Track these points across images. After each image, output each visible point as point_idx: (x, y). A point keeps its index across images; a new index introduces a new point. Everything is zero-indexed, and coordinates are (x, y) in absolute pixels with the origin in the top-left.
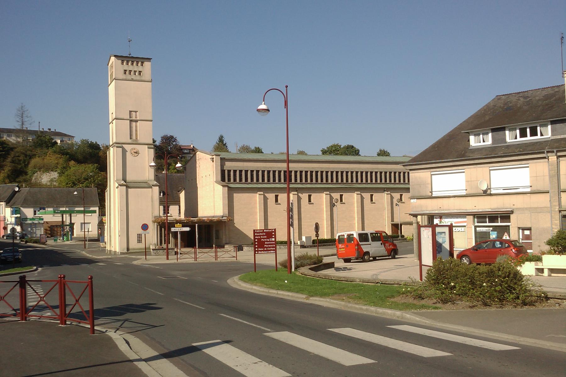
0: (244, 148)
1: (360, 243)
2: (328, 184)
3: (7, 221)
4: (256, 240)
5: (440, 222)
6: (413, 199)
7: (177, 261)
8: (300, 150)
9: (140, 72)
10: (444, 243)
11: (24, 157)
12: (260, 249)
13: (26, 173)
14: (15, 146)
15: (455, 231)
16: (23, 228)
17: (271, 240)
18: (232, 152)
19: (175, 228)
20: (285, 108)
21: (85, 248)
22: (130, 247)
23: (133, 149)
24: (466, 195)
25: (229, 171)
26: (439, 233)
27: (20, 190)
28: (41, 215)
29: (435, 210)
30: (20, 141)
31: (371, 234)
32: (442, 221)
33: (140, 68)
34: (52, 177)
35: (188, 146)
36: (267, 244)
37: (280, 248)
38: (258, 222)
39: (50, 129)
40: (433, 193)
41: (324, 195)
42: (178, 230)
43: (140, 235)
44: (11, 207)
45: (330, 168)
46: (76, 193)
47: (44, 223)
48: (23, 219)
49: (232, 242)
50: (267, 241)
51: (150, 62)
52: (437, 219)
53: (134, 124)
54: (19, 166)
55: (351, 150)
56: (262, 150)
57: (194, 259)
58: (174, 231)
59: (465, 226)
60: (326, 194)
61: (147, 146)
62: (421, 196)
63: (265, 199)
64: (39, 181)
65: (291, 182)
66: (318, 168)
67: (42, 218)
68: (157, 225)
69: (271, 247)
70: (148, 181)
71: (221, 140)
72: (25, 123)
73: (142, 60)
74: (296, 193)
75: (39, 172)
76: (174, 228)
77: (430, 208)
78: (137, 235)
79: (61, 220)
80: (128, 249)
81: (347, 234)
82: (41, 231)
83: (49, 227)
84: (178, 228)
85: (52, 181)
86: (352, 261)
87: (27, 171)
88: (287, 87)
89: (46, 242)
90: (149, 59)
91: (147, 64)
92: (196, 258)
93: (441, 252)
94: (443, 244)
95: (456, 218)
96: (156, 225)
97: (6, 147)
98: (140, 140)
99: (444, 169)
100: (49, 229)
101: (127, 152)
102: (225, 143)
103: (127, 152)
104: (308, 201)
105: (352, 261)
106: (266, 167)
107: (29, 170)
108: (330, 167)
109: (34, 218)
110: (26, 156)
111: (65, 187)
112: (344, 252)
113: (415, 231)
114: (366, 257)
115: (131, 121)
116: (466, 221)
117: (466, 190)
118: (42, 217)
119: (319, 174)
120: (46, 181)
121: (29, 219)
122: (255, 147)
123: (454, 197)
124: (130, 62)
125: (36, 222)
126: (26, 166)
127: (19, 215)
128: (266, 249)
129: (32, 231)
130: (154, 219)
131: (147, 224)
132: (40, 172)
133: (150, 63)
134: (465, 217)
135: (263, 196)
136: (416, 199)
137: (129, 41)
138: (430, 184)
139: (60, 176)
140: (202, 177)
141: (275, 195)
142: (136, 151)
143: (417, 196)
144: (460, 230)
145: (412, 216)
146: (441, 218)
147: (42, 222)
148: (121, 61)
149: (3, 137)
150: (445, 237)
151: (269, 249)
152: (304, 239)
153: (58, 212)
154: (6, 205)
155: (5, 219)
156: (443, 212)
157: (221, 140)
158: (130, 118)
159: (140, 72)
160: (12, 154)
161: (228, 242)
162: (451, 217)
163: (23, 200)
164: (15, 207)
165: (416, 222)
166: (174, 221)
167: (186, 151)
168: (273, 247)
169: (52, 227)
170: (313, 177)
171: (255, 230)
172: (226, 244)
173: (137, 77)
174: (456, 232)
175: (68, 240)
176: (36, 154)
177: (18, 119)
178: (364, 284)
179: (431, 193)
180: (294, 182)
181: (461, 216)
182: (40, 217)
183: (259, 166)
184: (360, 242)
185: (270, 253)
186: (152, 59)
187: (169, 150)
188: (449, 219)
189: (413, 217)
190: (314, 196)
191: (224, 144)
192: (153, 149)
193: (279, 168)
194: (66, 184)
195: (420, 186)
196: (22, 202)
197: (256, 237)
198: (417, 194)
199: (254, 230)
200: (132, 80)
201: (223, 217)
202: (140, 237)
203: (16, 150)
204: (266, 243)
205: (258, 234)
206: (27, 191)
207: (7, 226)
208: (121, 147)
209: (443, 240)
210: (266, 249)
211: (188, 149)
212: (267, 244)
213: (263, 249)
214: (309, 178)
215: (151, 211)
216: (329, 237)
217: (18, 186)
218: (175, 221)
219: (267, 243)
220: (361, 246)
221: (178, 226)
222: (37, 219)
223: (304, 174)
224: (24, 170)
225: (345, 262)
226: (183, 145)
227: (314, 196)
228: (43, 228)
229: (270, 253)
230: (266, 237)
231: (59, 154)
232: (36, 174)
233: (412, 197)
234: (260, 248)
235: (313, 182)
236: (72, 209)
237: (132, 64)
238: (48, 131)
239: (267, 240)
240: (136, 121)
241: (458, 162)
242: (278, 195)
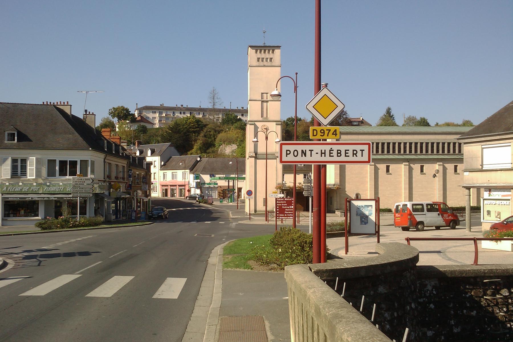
0: (411, 118)
1: (413, 213)
2: (445, 154)
3: (190, 185)
4: (278, 207)
5: (490, 195)
6: (465, 172)
7: (268, 223)
8: (466, 120)
9: (271, 59)
10: (371, 215)
11: (214, 133)
12: (281, 215)
13: (214, 145)
14: (208, 123)
15: (502, 204)
16: (202, 191)
17: (290, 207)
18: (432, 123)
20: (295, 92)
21: (238, 209)
22: (258, 209)
23: (264, 126)
24: (511, 169)
26: (366, 206)
27: (201, 160)
28: (215, 181)
29: (485, 183)
30: (212, 118)
31: (427, 205)
32: (491, 194)
33: (271, 55)
34: (233, 149)
35: (358, 119)
36: (287, 211)
37: (382, 215)
38: (368, 191)
39: (243, 108)
40: (484, 166)
41: (437, 165)
44: (193, 174)
45: (447, 139)
46: (231, 163)
47: (218, 187)
48: (203, 183)
50: (287, 209)
51: (280, 49)
52: (486, 191)
53: (265, 104)
54: (210, 140)
55: (424, 123)
56: (427, 121)
57: (281, 222)
59: (509, 200)
60: (404, 165)
61: (275, 123)
62: (473, 169)
63: (411, 170)
64: (223, 152)
65: (406, 153)
66: (434, 139)
67: (217, 183)
68: (280, 191)
69: (290, 214)
70: (275, 153)
71: (389, 111)
72: (216, 104)
73: (273, 48)
74: (407, 163)
75: (223, 145)
77: (480, 182)
78: (263, 199)
79: (232, 185)
80: (255, 211)
81: (402, 204)
82: (216, 194)
83: (222, 191)
85: (233, 152)
86: (410, 230)
87: (215, 144)
88: (297, 74)
89: (213, 203)
90: (278, 47)
91: (277, 52)
93: (368, 223)
94: (370, 217)
95: (503, 191)
96: (279, 191)
97: (201, 124)
98: (270, 118)
99: (489, 143)
100: (222, 192)
101: (258, 129)
102: (392, 115)
103: (259, 128)
104: (420, 172)
105: (410, 230)
106: (380, 140)
107: (217, 144)
108: (447, 138)
109: (210, 183)
110: (215, 131)
111: (240, 157)
112: (400, 221)
113: (467, 203)
114: (419, 226)
115: (263, 102)
116: (511, 195)
117: (512, 163)
118: (216, 182)
119: (435, 145)
120: (228, 152)
121: (206, 183)
122: (421, 118)
123: (501, 170)
124: (263, 51)
125: (212, 186)
126: (215, 139)
127: (199, 181)
128: (286, 215)
129: (208, 194)
130: (277, 186)
131: (251, 190)
132: (224, 144)
133: (280, 50)
134: (509, 191)
135: (408, 166)
136: (468, 172)
137: (264, 33)
138: (481, 158)
139: (238, 148)
141: (387, 166)
142: (266, 128)
143: (470, 169)
144: (506, 204)
145: (465, 189)
146: (490, 191)
147: (216, 186)
148: (255, 50)
149: (206, 116)
150: (372, 210)
151: (289, 215)
153: (223, 178)
154: (190, 171)
155: (189, 183)
156: (491, 185)
157: (389, 111)
158: (262, 99)
159: (271, 59)
160: (205, 130)
161: (339, 208)
162: (499, 191)
163: (203, 168)
164: (196, 174)
165: (469, 195)
166: (334, 188)
167: (355, 124)
168: (292, 214)
169: (224, 190)
170: (428, 148)
171: (277, 199)
172: (337, 210)
173: (269, 63)
174: (502, 205)
175: (231, 202)
176: (223, 129)
177: (210, 101)
179: (481, 166)
180: (408, 153)
181: (508, 190)
182: (215, 182)
183: (374, 138)
184: (413, 212)
185: (290, 218)
187: (340, 122)
188: (500, 192)
189: (466, 189)
190: (392, 167)
191: (391, 116)
192: (280, 125)
193: (394, 140)
194: (241, 155)
195: (472, 159)
196: (202, 169)
197: (278, 205)
198: (469, 167)
199: (276, 199)
200: (264, 66)
201: (334, 185)
203: (208, 127)
204: (286, 210)
205: (280, 202)
206: (206, 161)
207: (191, 189)
208: (253, 125)
209: (369, 213)
210: (286, 215)
211: (357, 121)
212: (287, 211)
213: (283, 215)
214: (435, 150)
216: (476, 205)
217: (200, 157)
218: (288, 188)
219: (287, 210)
220: (414, 216)
222: (213, 183)
223: (435, 145)
224: (214, 143)
225: (403, 231)
226: (352, 118)
227: (392, 167)
228: (217, 191)
229: (290, 218)
230: (286, 205)
231: (240, 129)
232: (221, 146)
233: (465, 170)
234: (281, 214)
235: (412, 153)
236: (228, 176)
237: (265, 52)
238: (241, 109)
239: (287, 207)
240: (267, 102)
241: (494, 137)
242: (389, 165)
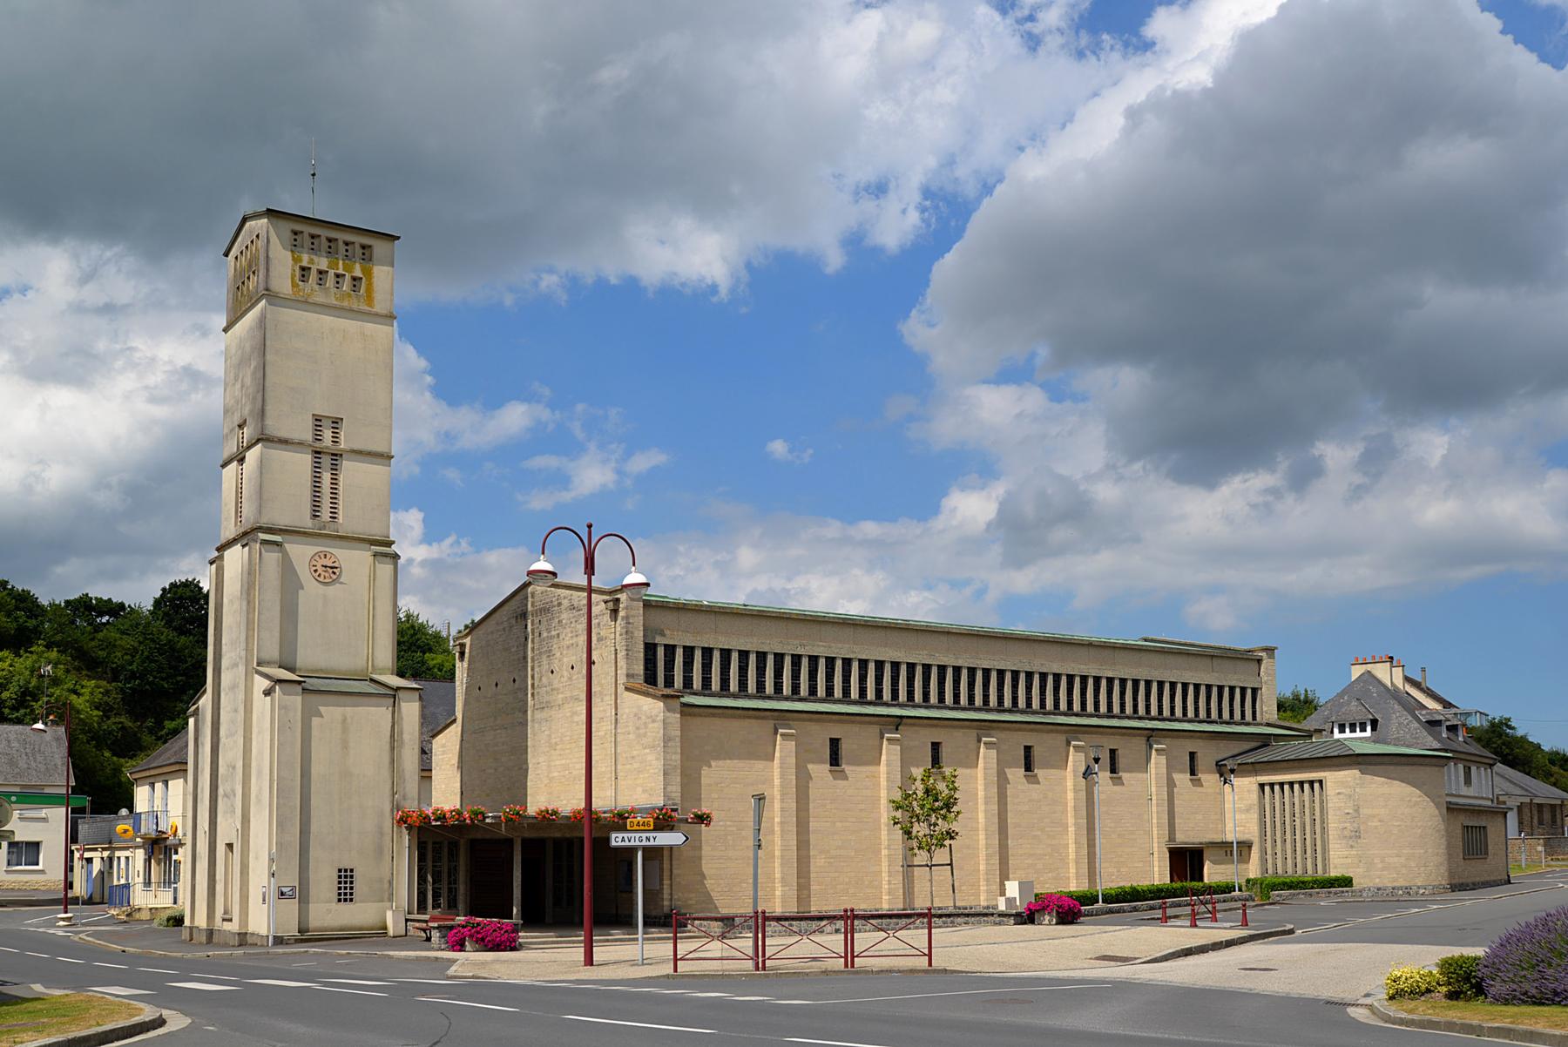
19: (626, 835)
25: (670, 650)
42: (638, 843)
43: (349, 873)
49: (690, 902)
58: (620, 844)
76: (620, 835)
78: (336, 874)
84: (638, 835)
92: (853, 957)
140: (497, 685)
152: (1012, 889)
178: (58, 1031)
186: (225, 330)
202: (346, 883)
215: (388, 786)
221: (638, 824)
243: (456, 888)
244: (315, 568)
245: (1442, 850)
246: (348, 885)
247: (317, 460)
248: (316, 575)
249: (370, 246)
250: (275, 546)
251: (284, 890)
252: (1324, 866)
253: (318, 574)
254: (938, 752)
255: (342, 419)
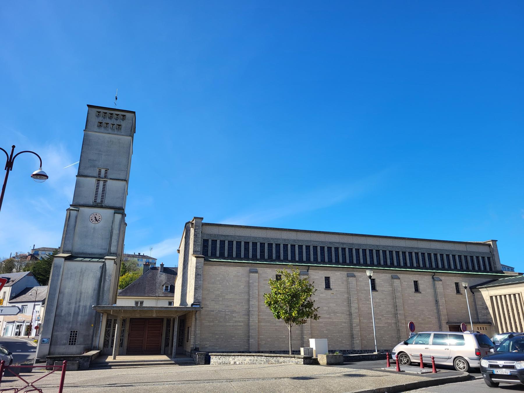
49: (206, 346)
243: (123, 339)
244: (91, 219)
245: (473, 245)
246: (74, 338)
247: (104, 183)
248: (92, 221)
249: (125, 115)
250: (76, 211)
251: (44, 339)
252: (103, 197)
253: (92, 220)
254: (329, 281)
255: (109, 169)
